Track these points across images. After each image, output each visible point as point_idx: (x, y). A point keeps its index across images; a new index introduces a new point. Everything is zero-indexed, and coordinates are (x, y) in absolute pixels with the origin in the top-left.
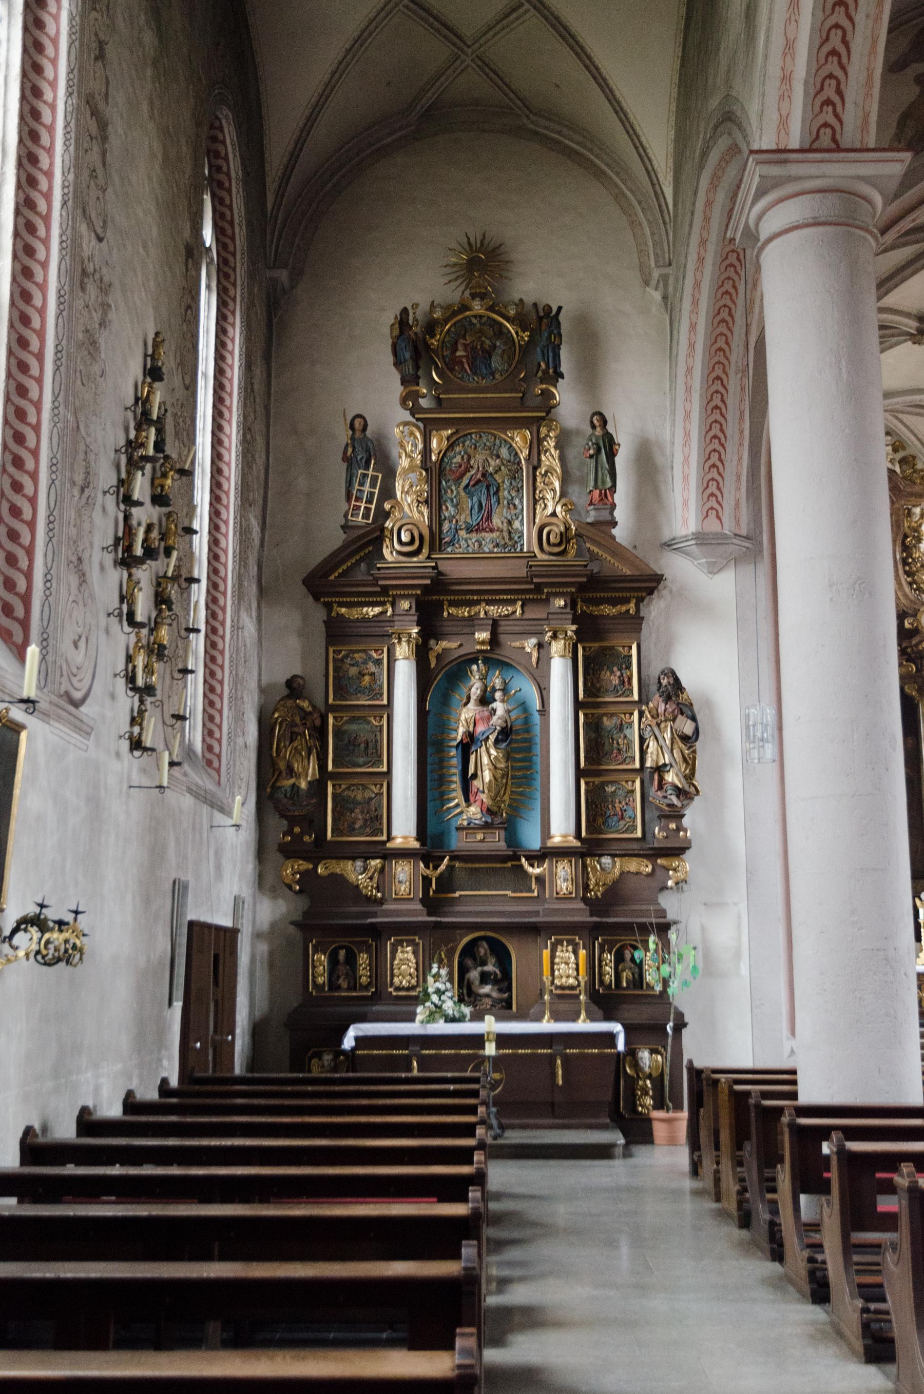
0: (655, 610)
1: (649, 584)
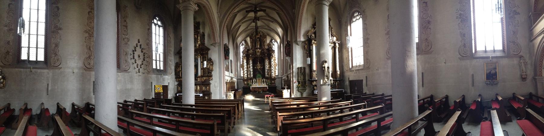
0: (210, 52)
1: (208, 49)
